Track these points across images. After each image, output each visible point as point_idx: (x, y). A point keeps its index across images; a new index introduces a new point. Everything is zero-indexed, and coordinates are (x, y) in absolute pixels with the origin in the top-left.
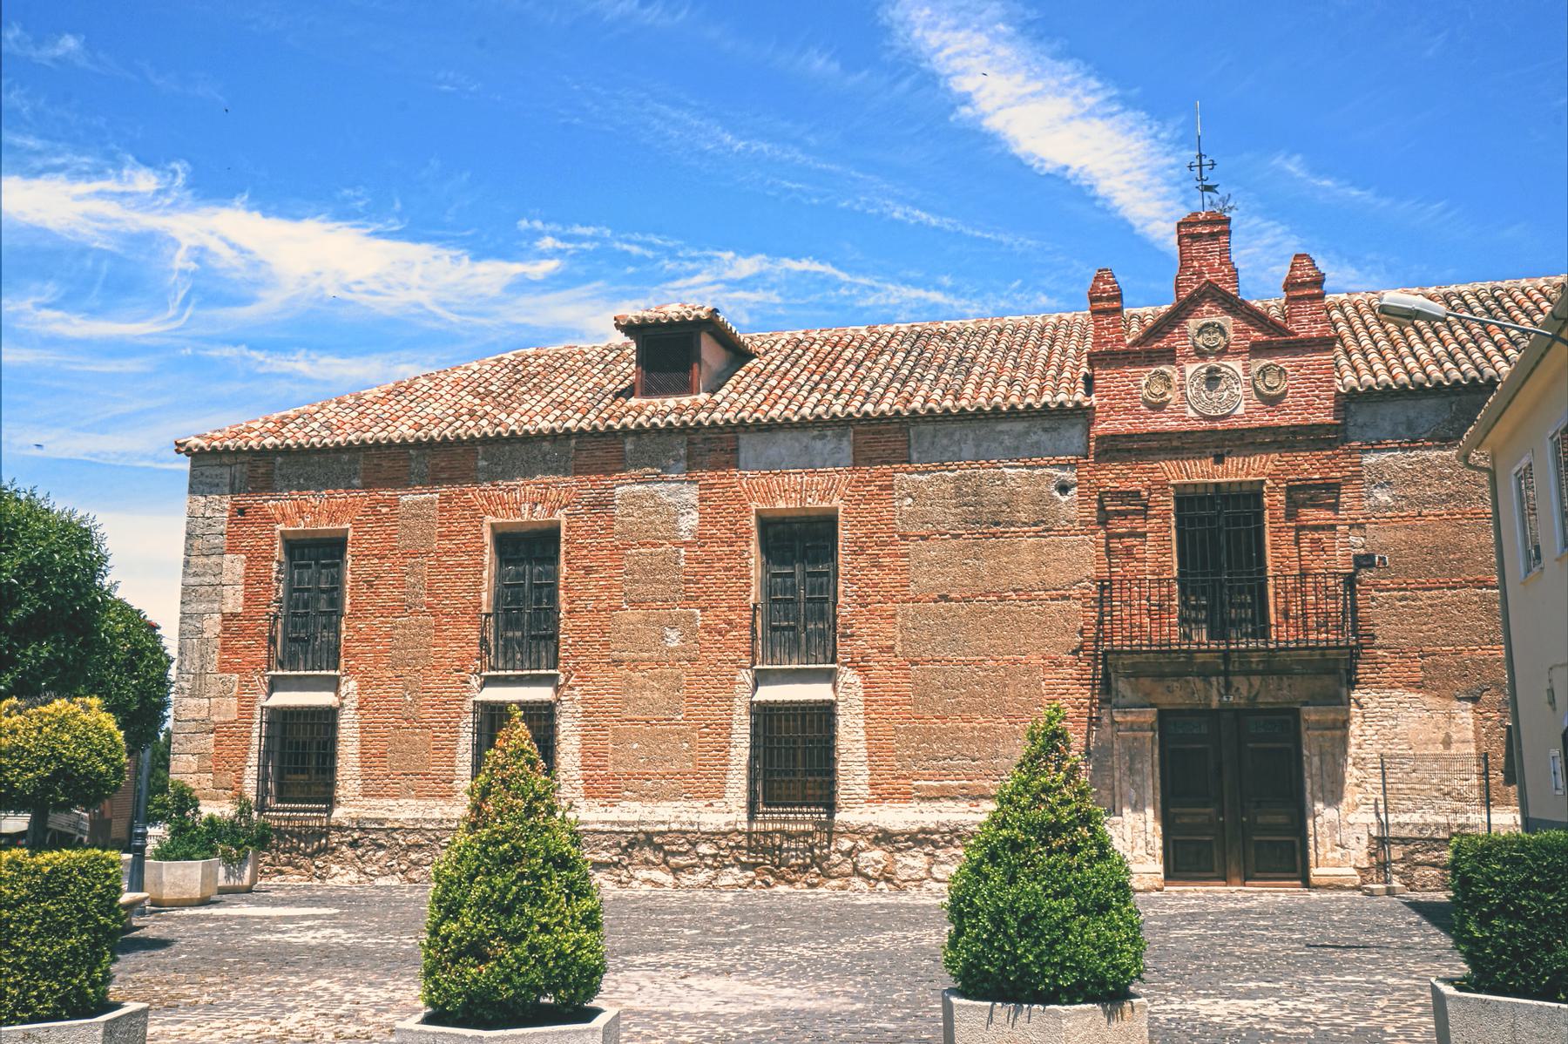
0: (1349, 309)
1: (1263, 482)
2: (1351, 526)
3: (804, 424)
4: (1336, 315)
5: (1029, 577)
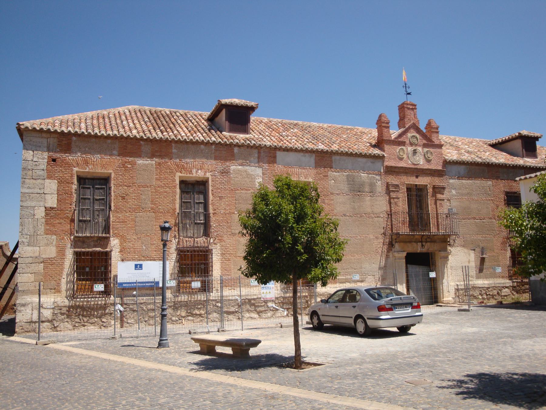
5: (369, 210)
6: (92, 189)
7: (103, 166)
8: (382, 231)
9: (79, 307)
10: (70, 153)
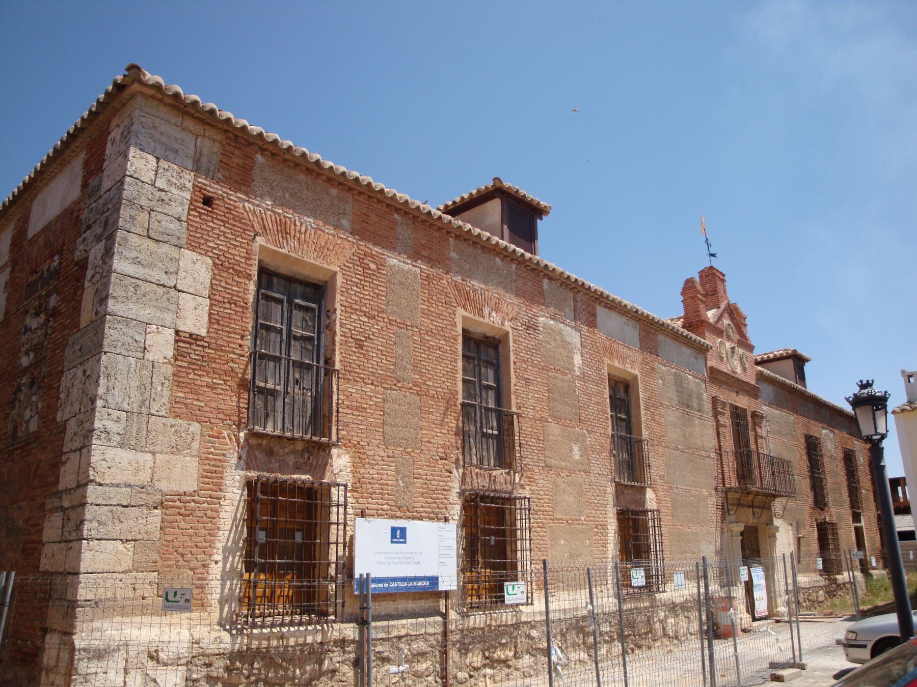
6: (286, 305)
7: (321, 250)
9: (258, 654)
10: (247, 194)
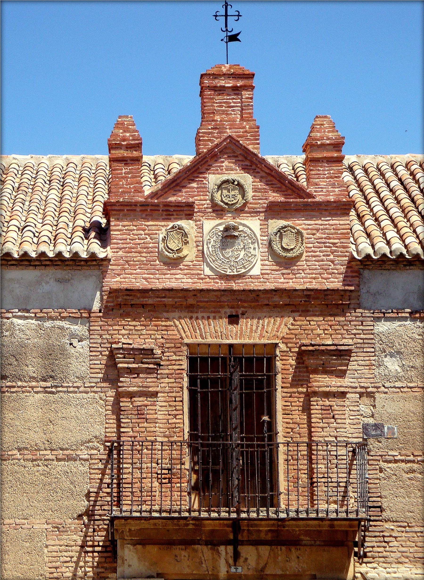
0: (360, 173)
1: (276, 345)
2: (361, 395)
3: (42, 261)
4: (347, 177)
5: (36, 437)
8: (83, 505)
